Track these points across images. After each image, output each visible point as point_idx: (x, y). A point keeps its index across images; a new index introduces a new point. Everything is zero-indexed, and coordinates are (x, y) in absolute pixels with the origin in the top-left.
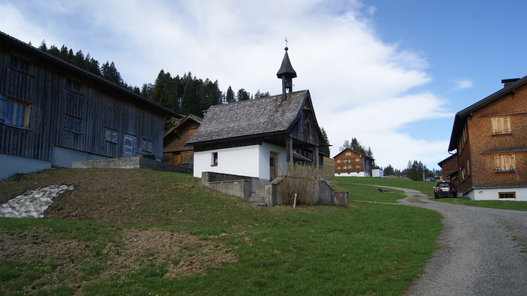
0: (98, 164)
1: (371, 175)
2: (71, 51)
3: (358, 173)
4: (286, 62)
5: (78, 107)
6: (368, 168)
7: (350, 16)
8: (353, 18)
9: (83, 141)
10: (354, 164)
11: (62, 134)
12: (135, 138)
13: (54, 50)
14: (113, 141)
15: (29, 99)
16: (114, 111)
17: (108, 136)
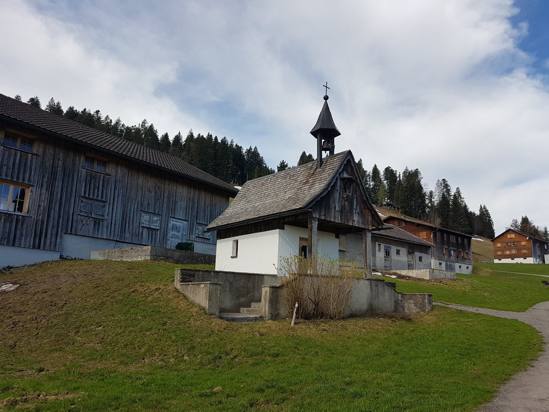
0: (113, 254)
1: (544, 261)
2: (216, 138)
3: (525, 258)
4: (326, 114)
5: (101, 189)
6: (539, 253)
7: (520, 74)
8: (524, 76)
9: (107, 227)
10: (519, 249)
11: (77, 220)
12: (185, 222)
13: (200, 138)
14: (154, 227)
15: (29, 181)
16: (156, 193)
17: (145, 221)
